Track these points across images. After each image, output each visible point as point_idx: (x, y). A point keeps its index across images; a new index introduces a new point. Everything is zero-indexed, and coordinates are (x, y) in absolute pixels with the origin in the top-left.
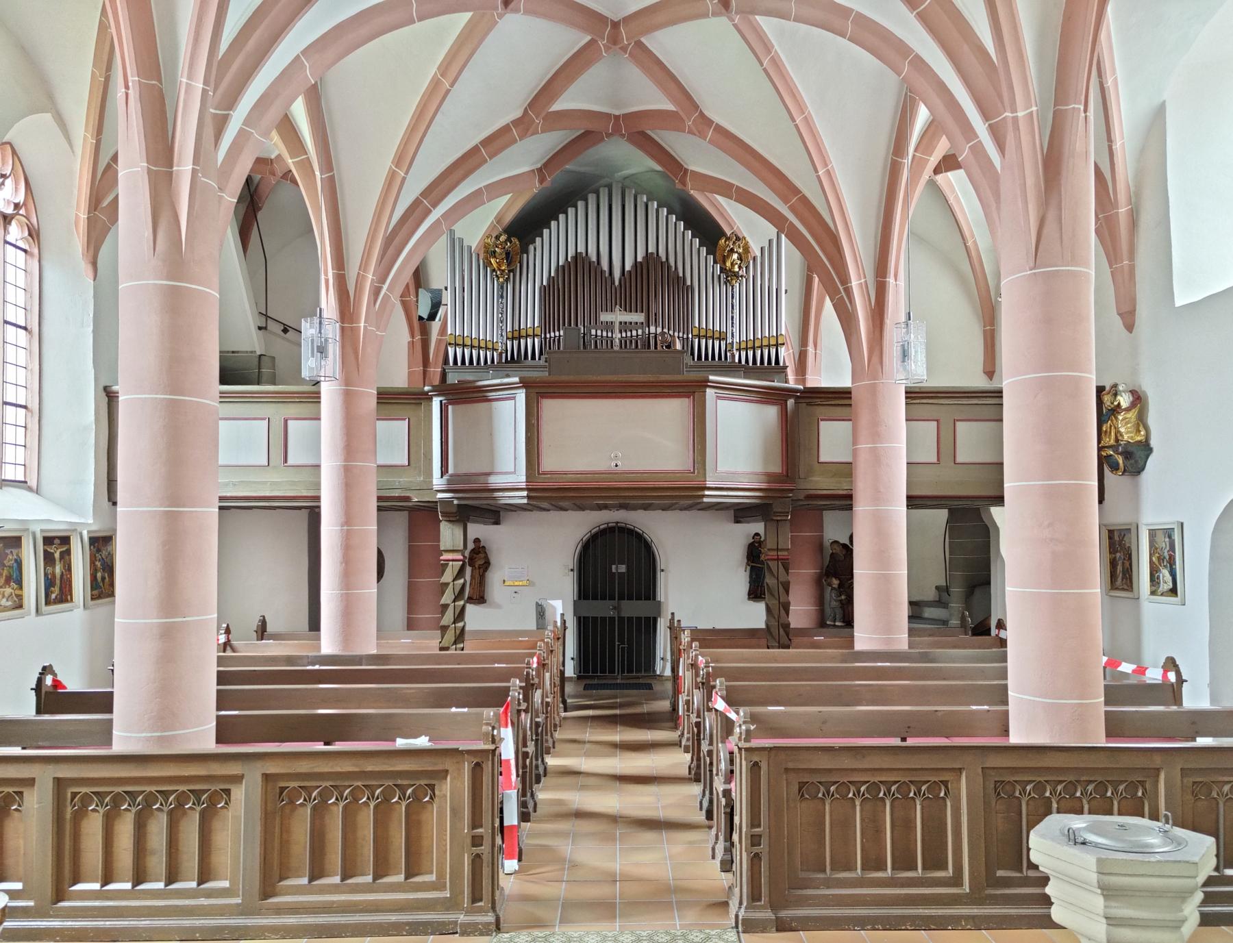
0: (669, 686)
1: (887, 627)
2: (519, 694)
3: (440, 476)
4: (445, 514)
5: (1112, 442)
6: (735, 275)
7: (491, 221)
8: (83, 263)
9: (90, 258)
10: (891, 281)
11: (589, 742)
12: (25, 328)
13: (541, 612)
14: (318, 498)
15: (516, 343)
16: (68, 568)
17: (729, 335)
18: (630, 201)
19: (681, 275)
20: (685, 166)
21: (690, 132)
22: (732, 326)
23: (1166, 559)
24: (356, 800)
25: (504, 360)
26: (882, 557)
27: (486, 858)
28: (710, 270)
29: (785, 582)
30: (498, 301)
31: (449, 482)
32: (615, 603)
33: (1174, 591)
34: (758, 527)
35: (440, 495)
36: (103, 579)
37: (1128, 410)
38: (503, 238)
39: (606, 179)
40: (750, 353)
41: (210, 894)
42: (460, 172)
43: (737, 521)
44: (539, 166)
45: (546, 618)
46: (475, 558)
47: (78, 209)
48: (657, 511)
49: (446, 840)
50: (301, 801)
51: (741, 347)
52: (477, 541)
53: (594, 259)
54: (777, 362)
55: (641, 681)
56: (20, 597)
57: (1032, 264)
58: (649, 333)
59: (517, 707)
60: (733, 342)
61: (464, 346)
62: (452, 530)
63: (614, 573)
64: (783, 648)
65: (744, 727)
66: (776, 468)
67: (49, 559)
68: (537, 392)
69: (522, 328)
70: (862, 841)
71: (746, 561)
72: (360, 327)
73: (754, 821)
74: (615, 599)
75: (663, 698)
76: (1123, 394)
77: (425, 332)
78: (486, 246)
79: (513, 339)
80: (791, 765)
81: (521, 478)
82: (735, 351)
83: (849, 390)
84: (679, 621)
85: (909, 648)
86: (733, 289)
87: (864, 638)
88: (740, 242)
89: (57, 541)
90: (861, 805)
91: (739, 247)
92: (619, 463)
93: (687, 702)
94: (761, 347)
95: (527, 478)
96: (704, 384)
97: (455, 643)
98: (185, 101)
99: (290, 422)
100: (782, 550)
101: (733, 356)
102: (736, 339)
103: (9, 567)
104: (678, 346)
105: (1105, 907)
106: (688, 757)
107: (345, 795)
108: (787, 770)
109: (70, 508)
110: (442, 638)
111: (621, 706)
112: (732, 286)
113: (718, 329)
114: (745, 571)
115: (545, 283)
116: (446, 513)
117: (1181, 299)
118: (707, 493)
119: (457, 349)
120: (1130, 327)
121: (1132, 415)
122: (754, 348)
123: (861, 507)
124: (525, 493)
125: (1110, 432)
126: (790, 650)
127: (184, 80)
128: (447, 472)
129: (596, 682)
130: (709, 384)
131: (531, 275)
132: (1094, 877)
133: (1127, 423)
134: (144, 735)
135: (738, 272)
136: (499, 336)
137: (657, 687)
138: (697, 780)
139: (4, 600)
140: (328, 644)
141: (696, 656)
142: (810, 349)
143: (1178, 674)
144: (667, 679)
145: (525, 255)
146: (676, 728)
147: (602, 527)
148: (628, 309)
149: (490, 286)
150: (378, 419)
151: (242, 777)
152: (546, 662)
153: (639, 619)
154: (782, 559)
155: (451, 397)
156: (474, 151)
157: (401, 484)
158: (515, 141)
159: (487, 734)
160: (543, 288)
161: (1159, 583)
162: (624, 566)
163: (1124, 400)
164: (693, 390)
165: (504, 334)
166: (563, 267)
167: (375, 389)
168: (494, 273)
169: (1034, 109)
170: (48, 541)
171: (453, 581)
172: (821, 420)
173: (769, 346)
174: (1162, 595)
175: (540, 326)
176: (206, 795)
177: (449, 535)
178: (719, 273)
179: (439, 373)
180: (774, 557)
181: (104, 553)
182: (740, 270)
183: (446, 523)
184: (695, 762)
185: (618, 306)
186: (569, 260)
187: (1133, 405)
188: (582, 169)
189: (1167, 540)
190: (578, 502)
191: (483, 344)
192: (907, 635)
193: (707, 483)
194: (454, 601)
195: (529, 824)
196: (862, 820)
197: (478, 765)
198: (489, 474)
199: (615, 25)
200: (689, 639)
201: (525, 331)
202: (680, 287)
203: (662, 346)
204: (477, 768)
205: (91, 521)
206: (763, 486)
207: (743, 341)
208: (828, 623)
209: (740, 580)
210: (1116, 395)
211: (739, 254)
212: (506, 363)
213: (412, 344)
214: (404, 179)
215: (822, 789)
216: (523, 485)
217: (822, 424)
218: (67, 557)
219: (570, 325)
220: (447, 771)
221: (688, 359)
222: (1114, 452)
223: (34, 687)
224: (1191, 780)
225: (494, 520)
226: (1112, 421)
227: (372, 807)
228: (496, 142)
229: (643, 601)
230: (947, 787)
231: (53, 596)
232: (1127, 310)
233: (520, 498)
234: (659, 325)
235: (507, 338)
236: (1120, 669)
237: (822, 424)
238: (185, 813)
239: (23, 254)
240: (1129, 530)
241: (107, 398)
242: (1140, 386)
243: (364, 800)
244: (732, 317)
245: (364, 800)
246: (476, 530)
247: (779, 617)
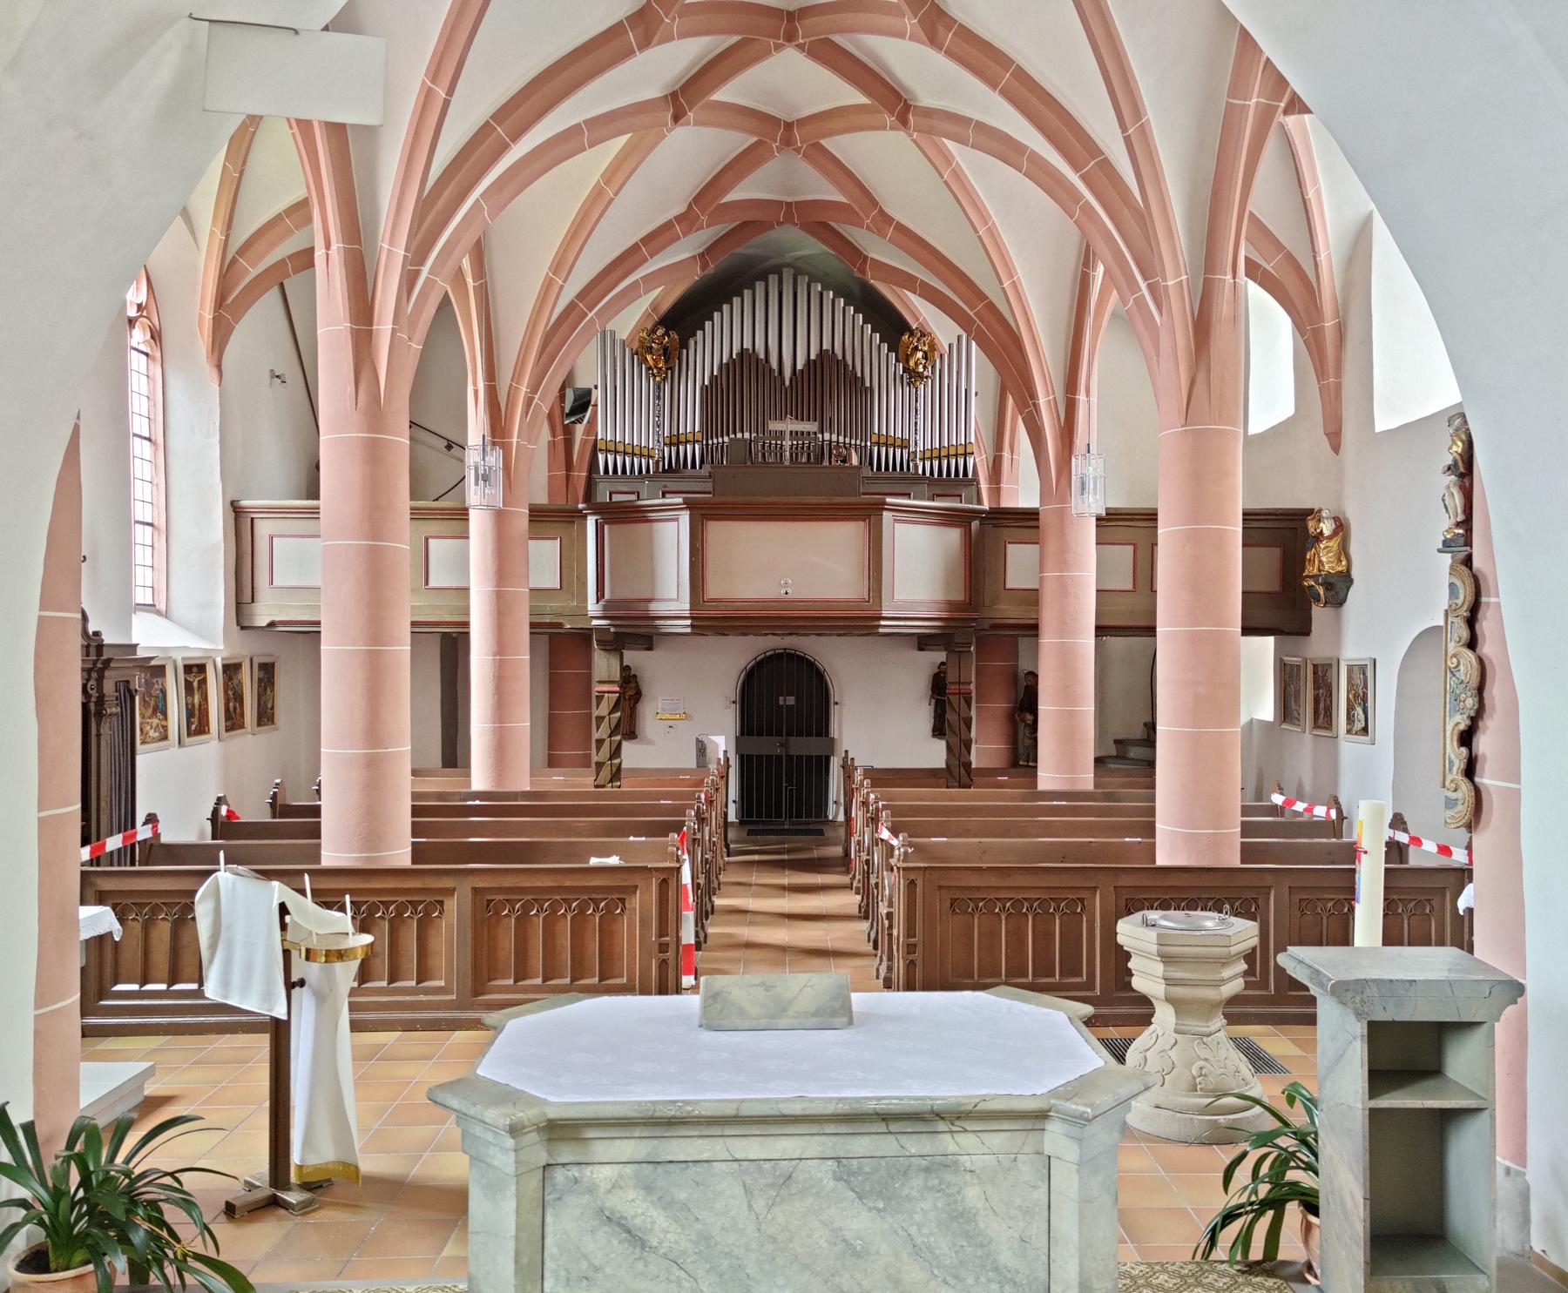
0: (842, 832)
1: (1071, 766)
2: (694, 824)
5: (1315, 571)
7: (645, 309)
8: (207, 366)
9: (215, 362)
10: (1081, 398)
11: (755, 885)
12: (149, 439)
13: (701, 749)
14: (466, 624)
15: (674, 449)
16: (205, 698)
18: (803, 290)
19: (859, 375)
22: (916, 434)
23: (1360, 698)
24: (555, 912)
25: (661, 470)
26: (1068, 693)
27: (671, 963)
30: (654, 403)
31: (605, 608)
33: (1365, 730)
34: (941, 656)
35: (595, 622)
36: (235, 708)
37: (1330, 538)
38: (660, 332)
39: (774, 260)
40: (936, 463)
41: (428, 991)
43: (921, 649)
44: (701, 250)
45: (708, 755)
47: (202, 307)
49: (635, 948)
50: (506, 912)
53: (762, 356)
55: (811, 827)
56: (165, 728)
57: (1183, 422)
58: (823, 441)
59: (693, 837)
60: (916, 451)
62: (608, 661)
64: (963, 788)
65: (902, 850)
66: (959, 596)
67: (189, 687)
68: (702, 513)
70: (1006, 950)
71: (930, 693)
72: (512, 442)
73: (910, 932)
75: (836, 844)
76: (1326, 521)
77: (568, 431)
80: (943, 883)
81: (684, 606)
83: (1036, 511)
84: (853, 759)
85: (1095, 787)
86: (916, 391)
87: (1047, 779)
88: (925, 339)
89: (195, 669)
90: (1006, 919)
91: (924, 345)
92: (789, 591)
93: (859, 843)
94: (948, 456)
96: (880, 507)
97: (611, 781)
98: (386, 265)
99: (431, 541)
100: (963, 683)
101: (916, 467)
102: (920, 448)
103: (156, 697)
104: (855, 461)
105: (1164, 971)
106: (859, 898)
107: (545, 907)
108: (940, 887)
109: (199, 632)
110: (598, 775)
111: (789, 851)
112: (917, 388)
117: (1381, 425)
118: (883, 623)
120: (1336, 448)
121: (1334, 544)
122: (939, 458)
123: (1047, 640)
124: (688, 622)
125: (1314, 561)
126: (972, 789)
127: (386, 246)
128: (603, 597)
129: (761, 827)
131: (691, 373)
132: (1154, 948)
133: (1328, 552)
134: (353, 855)
136: (656, 442)
137: (829, 833)
138: (866, 918)
139: (152, 731)
140: (479, 779)
141: (868, 793)
142: (1006, 454)
143: (1339, 811)
144: (840, 824)
145: (685, 351)
146: (848, 872)
147: (768, 654)
148: (799, 417)
149: (647, 386)
150: (531, 538)
151: (454, 889)
152: (714, 798)
153: (809, 758)
154: (964, 694)
155: (607, 516)
156: (634, 248)
157: (553, 608)
158: (678, 238)
159: (673, 853)
160: (704, 388)
161: (1354, 722)
162: (793, 698)
163: (1327, 528)
164: (869, 512)
166: (727, 364)
167: (527, 507)
169: (1184, 277)
170: (188, 669)
171: (610, 714)
172: (1009, 543)
173: (956, 455)
174: (1356, 733)
176: (422, 906)
177: (604, 666)
179: (584, 479)
180: (955, 691)
181: (235, 681)
184: (865, 900)
185: (788, 416)
186: (734, 357)
187: (1335, 533)
189: (1362, 676)
191: (637, 451)
192: (1092, 775)
194: (610, 736)
195: (700, 953)
196: (1007, 932)
197: (664, 881)
198: (650, 600)
199: (789, 126)
200: (862, 777)
202: (858, 389)
204: (664, 884)
205: (221, 647)
206: (944, 615)
208: (1021, 763)
209: (923, 716)
210: (1319, 521)
211: (925, 353)
213: (552, 445)
214: (562, 287)
215: (972, 905)
216: (687, 614)
217: (1010, 547)
218: (204, 686)
220: (636, 887)
221: (866, 472)
222: (1314, 581)
223: (210, 817)
224: (1298, 897)
226: (1316, 549)
227: (569, 918)
228: (657, 239)
229: (1383, 866)
230: (1083, 904)
231: (193, 727)
232: (1333, 431)
233: (683, 626)
235: (665, 444)
236: (1294, 808)
237: (1010, 547)
238: (403, 921)
239: (144, 357)
240: (1330, 665)
241: (234, 514)
242: (1344, 513)
243: (562, 911)
244: (916, 423)
245: (562, 911)
246: (632, 657)
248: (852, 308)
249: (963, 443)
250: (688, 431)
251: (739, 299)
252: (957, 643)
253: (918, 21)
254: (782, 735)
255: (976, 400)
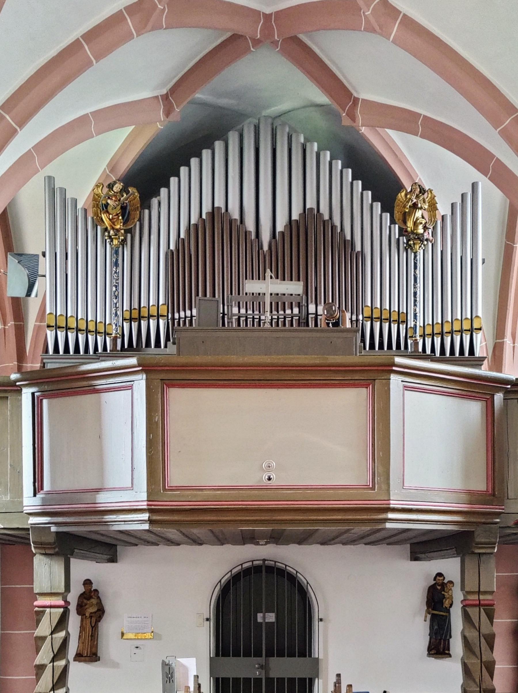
3: (32, 495)
4: (40, 545)
6: (419, 238)
15: (134, 325)
17: (411, 317)
19: (348, 237)
20: (355, 95)
21: (370, 29)
22: (415, 305)
25: (119, 347)
28: (386, 232)
29: (489, 635)
32: (261, 660)
38: (118, 187)
40: (438, 341)
42: (55, 78)
43: (414, 557)
44: (164, 91)
46: (85, 605)
48: (313, 545)
51: (426, 333)
52: (88, 583)
53: (236, 215)
54: (472, 351)
60: (415, 325)
61: (67, 329)
63: (261, 623)
69: (142, 306)
74: (261, 656)
78: (96, 198)
79: (131, 320)
82: (418, 338)
86: (415, 257)
91: (424, 202)
94: (451, 333)
95: (148, 496)
100: (485, 593)
101: (416, 343)
112: (415, 253)
113: (397, 310)
114: (425, 621)
115: (172, 247)
116: (36, 542)
119: (59, 333)
122: (442, 334)
124: (145, 516)
128: (42, 489)
130: (394, 368)
131: (154, 237)
135: (422, 235)
145: (147, 211)
147: (245, 566)
155: (46, 388)
160: (170, 254)
165: (119, 313)
166: (196, 226)
168: (106, 234)
171: (52, 633)
173: (461, 331)
175: (166, 304)
178: (397, 237)
180: (474, 602)
182: (425, 231)
183: (42, 557)
185: (268, 270)
186: (204, 216)
188: (223, 102)
190: (217, 529)
191: (91, 327)
193: (392, 502)
194: (53, 660)
198: (98, 491)
201: (147, 310)
203: (328, 324)
207: (428, 324)
212: (121, 350)
216: (144, 505)
219: (205, 295)
225: (109, 557)
234: (320, 303)
235: (124, 319)
244: (415, 294)
247: (481, 680)
248: (340, 162)
249: (469, 317)
250: (151, 304)
251: (210, 151)
252: (478, 544)
253: (346, 114)
254: (261, 656)
255: (483, 269)
